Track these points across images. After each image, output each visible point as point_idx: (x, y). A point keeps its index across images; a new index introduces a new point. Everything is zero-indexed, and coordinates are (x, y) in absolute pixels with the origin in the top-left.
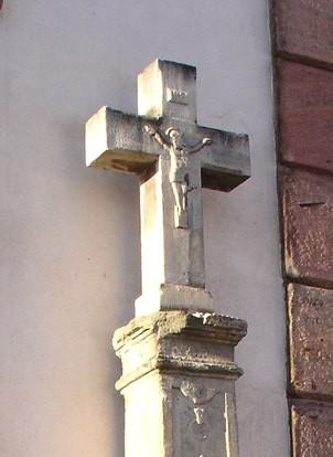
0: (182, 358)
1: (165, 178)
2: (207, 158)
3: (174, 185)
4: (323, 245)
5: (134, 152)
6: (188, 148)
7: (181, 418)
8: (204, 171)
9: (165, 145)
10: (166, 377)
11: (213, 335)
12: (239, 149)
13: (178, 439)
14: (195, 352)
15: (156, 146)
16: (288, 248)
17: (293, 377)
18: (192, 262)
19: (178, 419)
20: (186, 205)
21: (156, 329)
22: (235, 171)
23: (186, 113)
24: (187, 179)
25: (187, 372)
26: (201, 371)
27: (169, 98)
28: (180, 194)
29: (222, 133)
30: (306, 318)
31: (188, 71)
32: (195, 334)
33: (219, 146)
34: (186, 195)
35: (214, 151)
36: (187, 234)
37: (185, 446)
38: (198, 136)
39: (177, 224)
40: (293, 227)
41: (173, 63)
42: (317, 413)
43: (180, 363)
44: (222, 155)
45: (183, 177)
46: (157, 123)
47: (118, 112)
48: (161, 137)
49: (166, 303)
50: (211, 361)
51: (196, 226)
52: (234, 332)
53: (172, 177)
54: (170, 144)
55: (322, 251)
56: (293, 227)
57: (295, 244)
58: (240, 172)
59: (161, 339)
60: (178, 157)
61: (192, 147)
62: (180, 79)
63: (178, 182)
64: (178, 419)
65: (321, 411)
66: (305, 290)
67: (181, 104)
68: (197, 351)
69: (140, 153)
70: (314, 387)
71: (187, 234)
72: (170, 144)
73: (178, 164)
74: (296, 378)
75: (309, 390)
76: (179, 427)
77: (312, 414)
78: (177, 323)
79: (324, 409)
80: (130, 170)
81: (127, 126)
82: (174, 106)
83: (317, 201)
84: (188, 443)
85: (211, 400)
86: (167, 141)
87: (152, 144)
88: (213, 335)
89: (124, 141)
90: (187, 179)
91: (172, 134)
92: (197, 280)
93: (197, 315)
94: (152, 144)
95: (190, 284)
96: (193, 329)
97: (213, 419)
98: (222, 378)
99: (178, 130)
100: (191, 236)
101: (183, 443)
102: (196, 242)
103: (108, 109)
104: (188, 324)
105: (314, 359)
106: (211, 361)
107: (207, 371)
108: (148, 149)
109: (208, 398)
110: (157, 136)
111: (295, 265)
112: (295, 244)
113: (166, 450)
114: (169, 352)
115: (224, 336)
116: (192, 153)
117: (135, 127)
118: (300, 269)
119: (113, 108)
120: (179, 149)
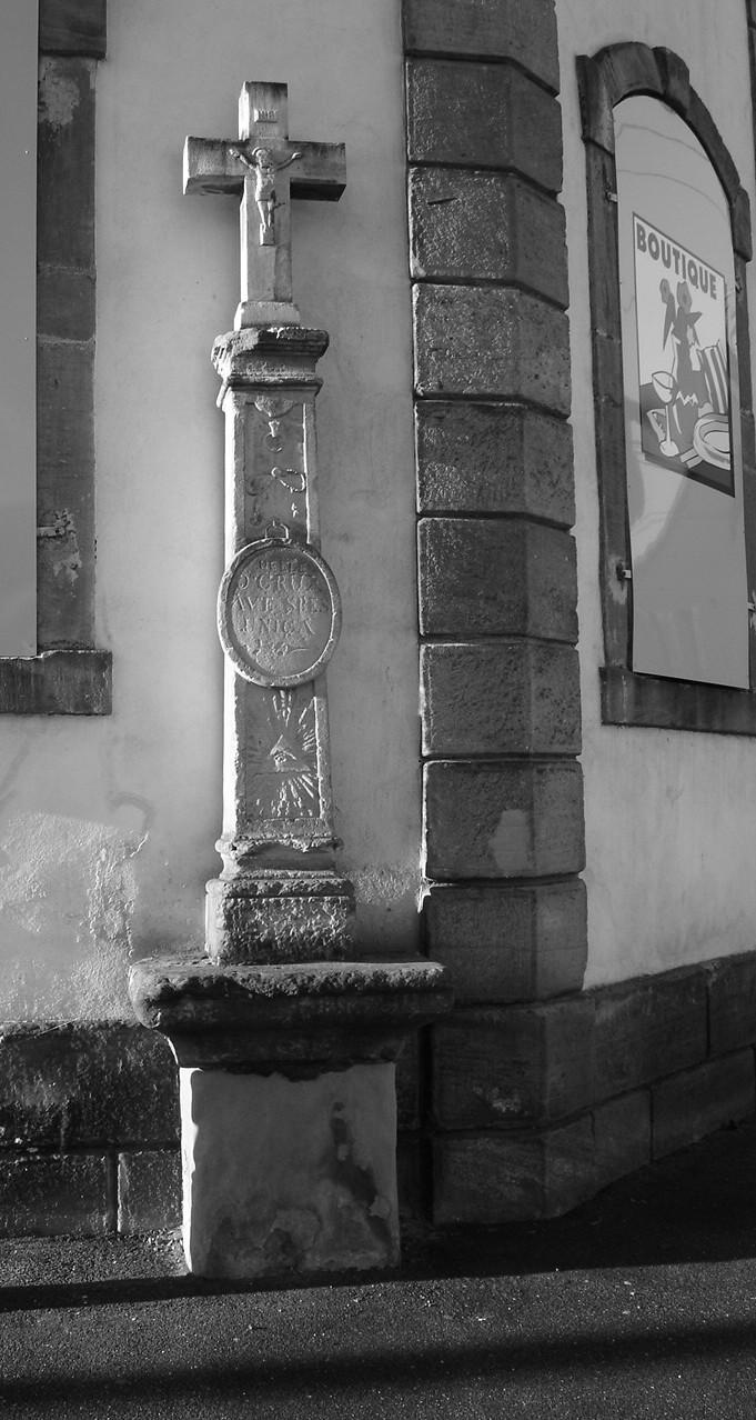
0: (252, 374)
1: (251, 197)
2: (297, 172)
3: (259, 203)
4: (454, 242)
5: (218, 176)
6: (276, 164)
7: (255, 433)
8: (293, 186)
9: (250, 166)
10: (239, 394)
11: (288, 348)
12: (335, 158)
13: (251, 455)
14: (271, 368)
15: (241, 167)
16: (414, 249)
17: (416, 379)
18: (278, 278)
19: (252, 437)
20: (272, 221)
21: (230, 348)
22: (329, 181)
23: (275, 130)
24: (273, 197)
25: (261, 387)
26: (275, 385)
27: (256, 118)
28: (266, 212)
29: (315, 146)
30: (432, 317)
31: (278, 89)
32: (269, 348)
33: (311, 157)
34: (272, 212)
35: (305, 165)
36: (274, 249)
37: (259, 460)
38: (287, 152)
39: (262, 243)
40: (420, 226)
41: (263, 83)
42: (444, 413)
43: (252, 379)
44: (315, 166)
45: (270, 194)
46: (243, 146)
47: (202, 139)
48: (246, 157)
49: (248, 321)
50: (288, 374)
51: (284, 240)
52: (311, 343)
53: (257, 197)
54: (255, 164)
55: (453, 247)
56: (420, 226)
57: (421, 245)
58: (334, 181)
59: (235, 356)
60: (264, 175)
61: (280, 164)
62: (269, 98)
63: (264, 200)
64: (252, 437)
65: (448, 412)
66: (433, 290)
67: (270, 122)
68: (274, 365)
69: (225, 176)
70: (441, 386)
71: (274, 249)
72: (255, 164)
73: (263, 183)
74: (420, 380)
75: (435, 390)
76: (252, 443)
77: (438, 414)
78: (250, 340)
79: (453, 409)
80: (226, 193)
81: (209, 152)
82: (262, 125)
83: (448, 197)
84: (261, 456)
85: (288, 411)
86: (252, 161)
87: (237, 166)
88: (288, 348)
89: (207, 167)
90: (273, 197)
91: (257, 152)
92: (283, 294)
93: (272, 330)
94: (237, 166)
95: (276, 300)
96: (267, 345)
97: (290, 432)
98: (301, 390)
99: (265, 149)
100: (277, 252)
101: (256, 457)
102: (283, 256)
103: (190, 139)
104: (260, 340)
105: (441, 358)
106: (288, 374)
107: (281, 385)
108: (233, 171)
109: (285, 410)
110: (241, 157)
111: (421, 266)
112: (421, 245)
113: (236, 464)
114: (243, 367)
115: (301, 348)
116: (281, 169)
117: (219, 152)
118: (427, 269)
119: (196, 136)
120: (265, 167)
